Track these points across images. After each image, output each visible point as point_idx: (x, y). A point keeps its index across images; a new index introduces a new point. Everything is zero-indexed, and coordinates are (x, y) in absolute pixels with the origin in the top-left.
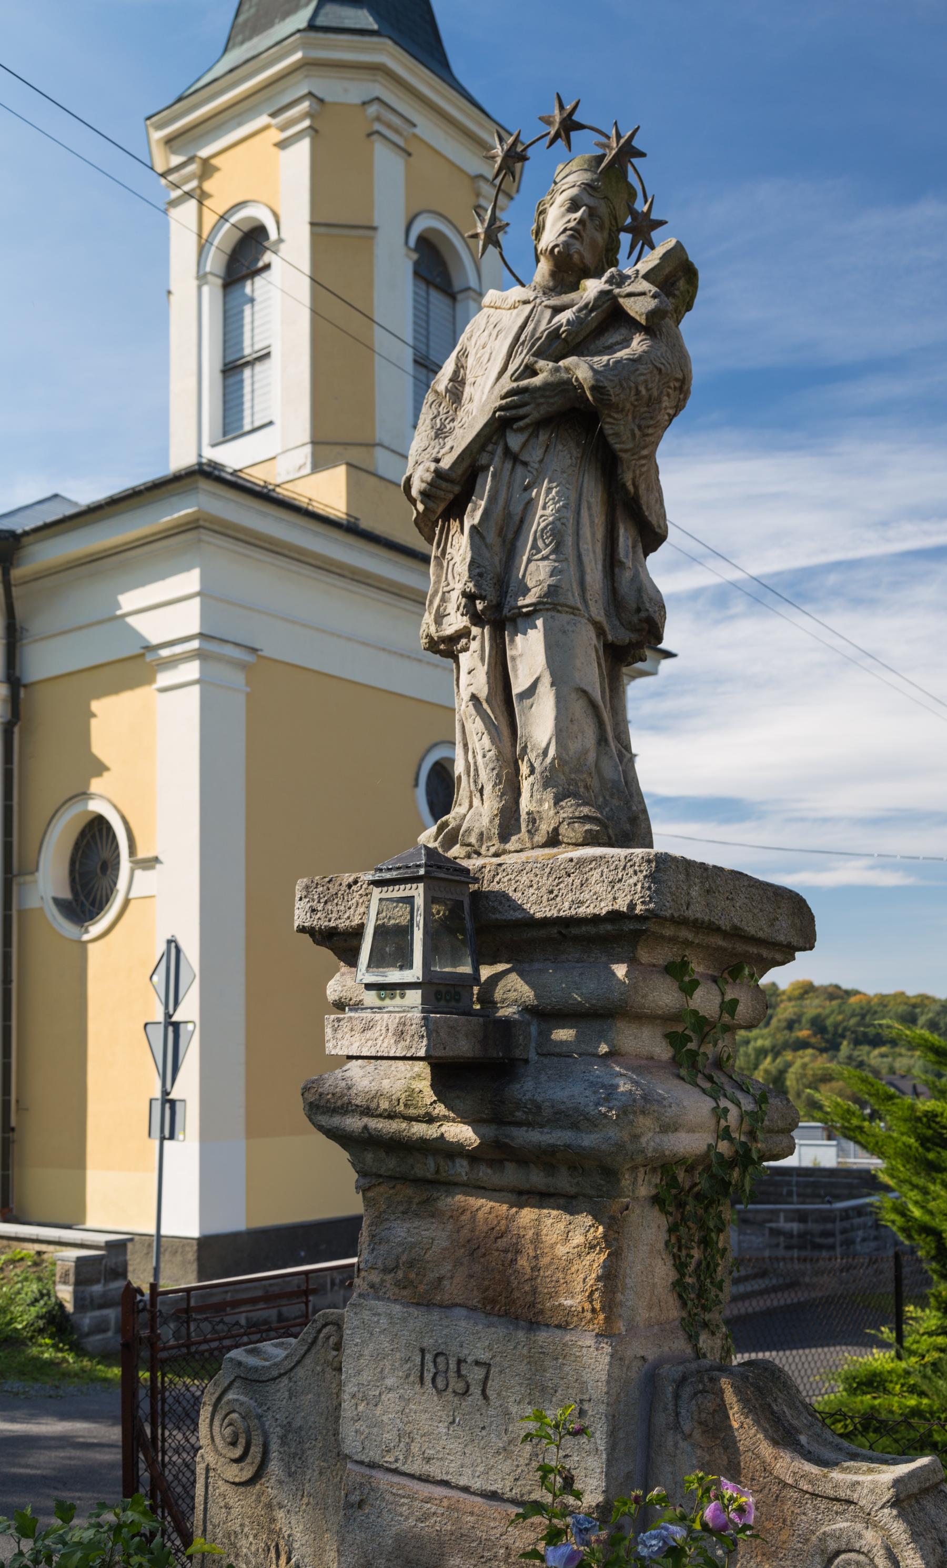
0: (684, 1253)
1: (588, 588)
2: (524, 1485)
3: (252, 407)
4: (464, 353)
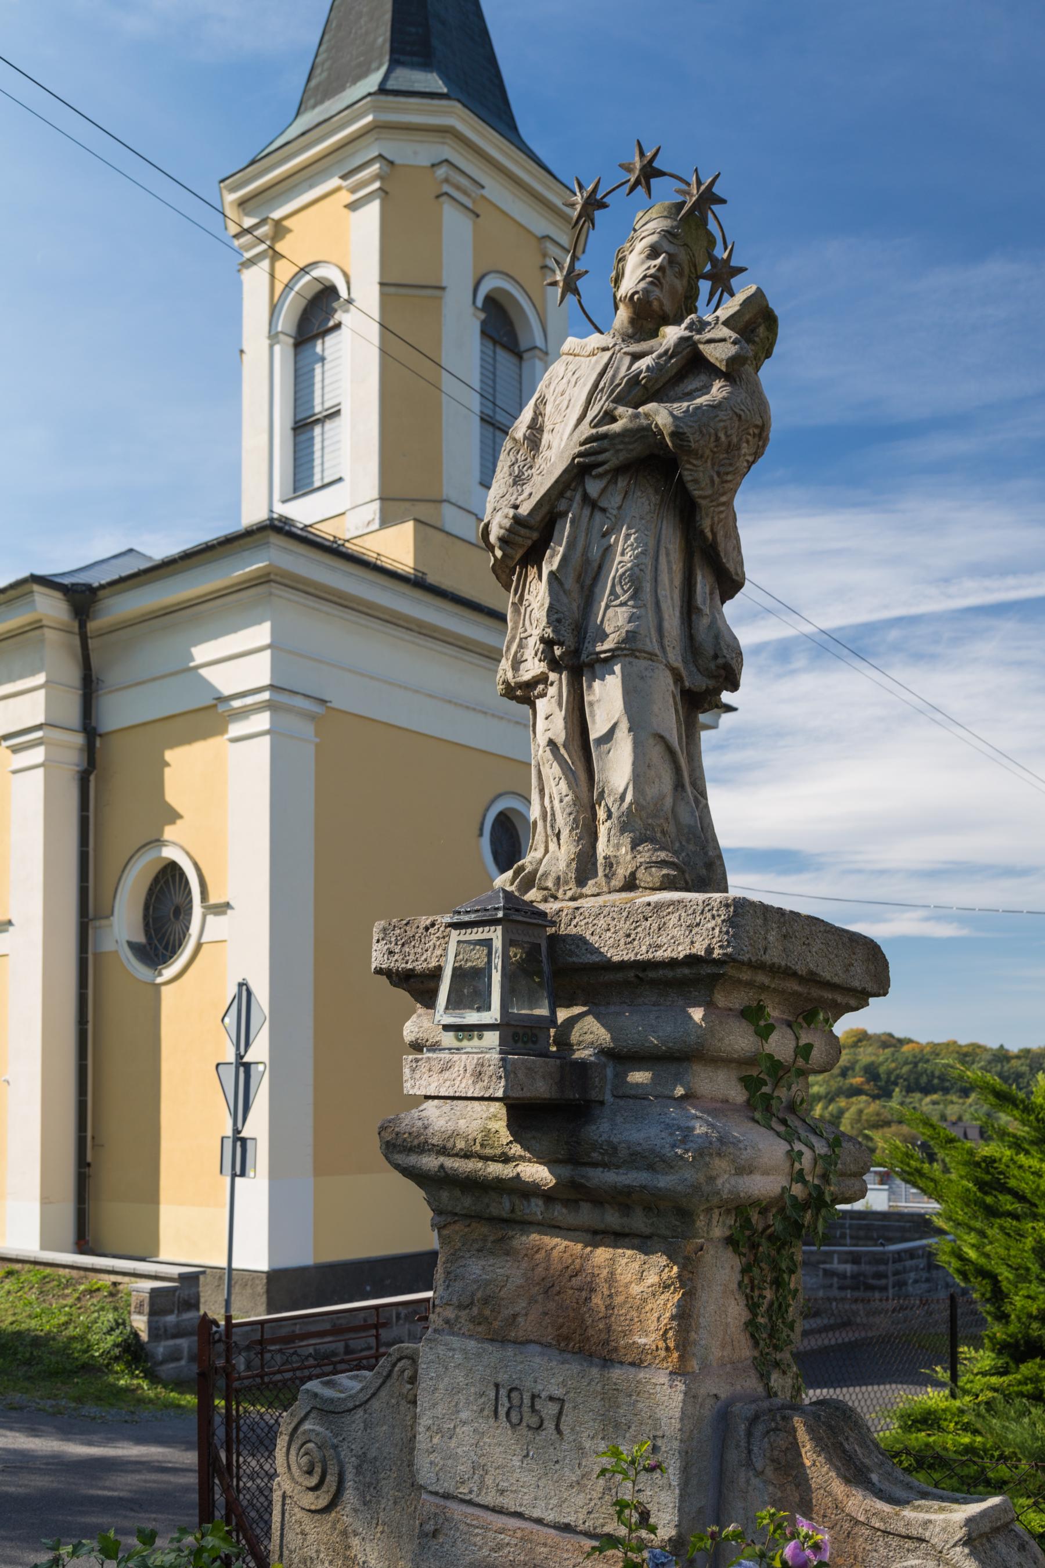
0: (756, 1293)
1: (666, 634)
2: (597, 1518)
3: (322, 464)
4: (542, 401)
